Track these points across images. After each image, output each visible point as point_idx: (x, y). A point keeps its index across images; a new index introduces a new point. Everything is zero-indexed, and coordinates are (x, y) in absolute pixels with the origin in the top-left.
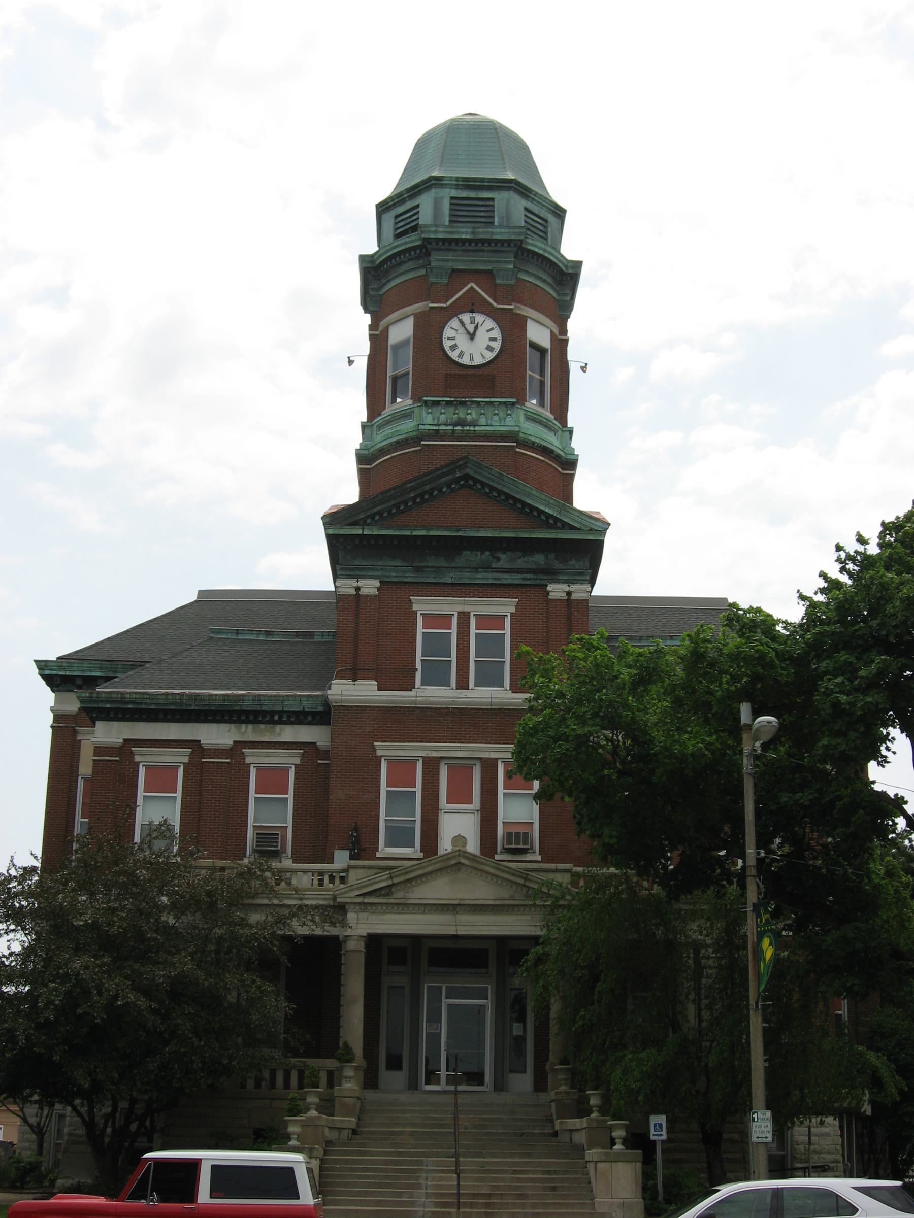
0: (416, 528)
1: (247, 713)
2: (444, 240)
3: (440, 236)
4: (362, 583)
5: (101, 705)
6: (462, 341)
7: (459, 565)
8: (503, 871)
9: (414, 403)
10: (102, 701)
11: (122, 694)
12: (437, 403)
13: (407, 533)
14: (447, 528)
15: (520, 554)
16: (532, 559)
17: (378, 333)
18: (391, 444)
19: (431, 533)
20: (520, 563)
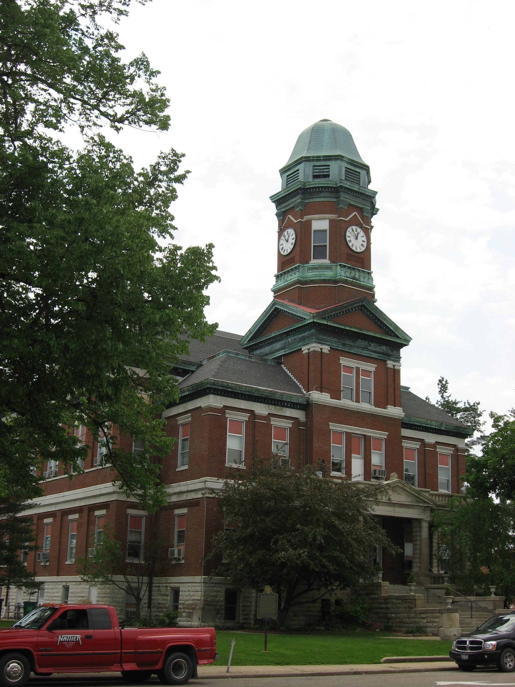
0: (347, 326)
1: (275, 400)
2: (347, 189)
3: (347, 186)
4: (323, 347)
5: (217, 387)
6: (352, 238)
7: (357, 345)
8: (412, 490)
9: (331, 263)
10: (218, 385)
11: (228, 383)
12: (345, 266)
13: (343, 328)
14: (357, 328)
15: (378, 345)
16: (382, 348)
17: (303, 221)
18: (320, 280)
19: (352, 329)
20: (378, 349)
